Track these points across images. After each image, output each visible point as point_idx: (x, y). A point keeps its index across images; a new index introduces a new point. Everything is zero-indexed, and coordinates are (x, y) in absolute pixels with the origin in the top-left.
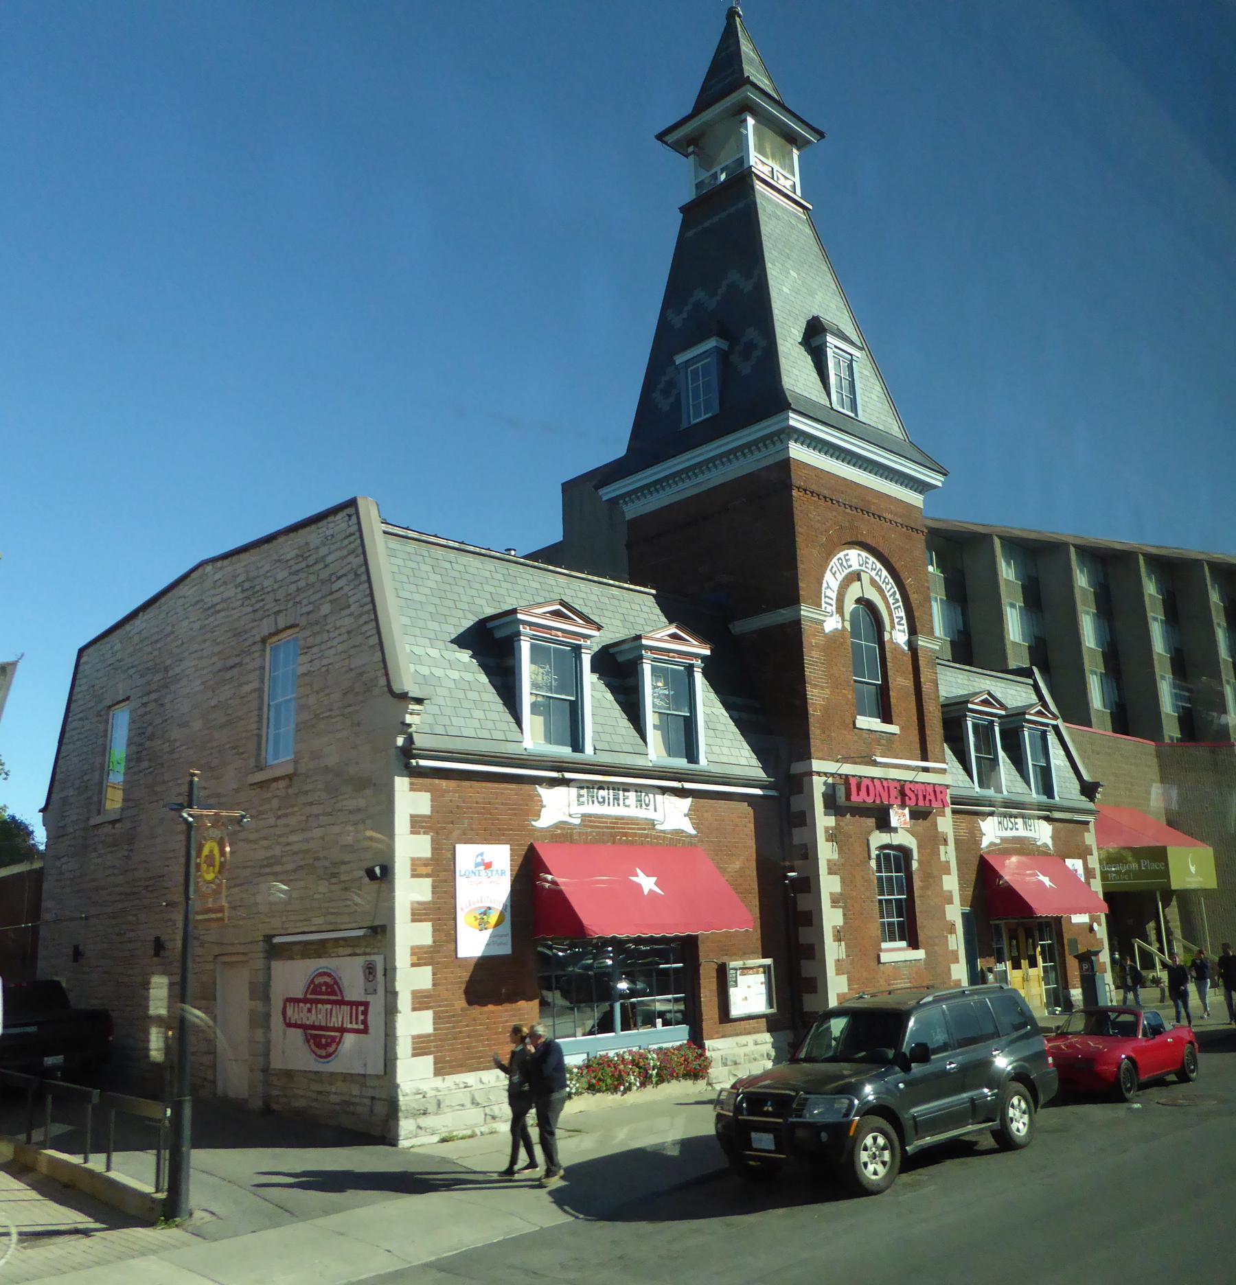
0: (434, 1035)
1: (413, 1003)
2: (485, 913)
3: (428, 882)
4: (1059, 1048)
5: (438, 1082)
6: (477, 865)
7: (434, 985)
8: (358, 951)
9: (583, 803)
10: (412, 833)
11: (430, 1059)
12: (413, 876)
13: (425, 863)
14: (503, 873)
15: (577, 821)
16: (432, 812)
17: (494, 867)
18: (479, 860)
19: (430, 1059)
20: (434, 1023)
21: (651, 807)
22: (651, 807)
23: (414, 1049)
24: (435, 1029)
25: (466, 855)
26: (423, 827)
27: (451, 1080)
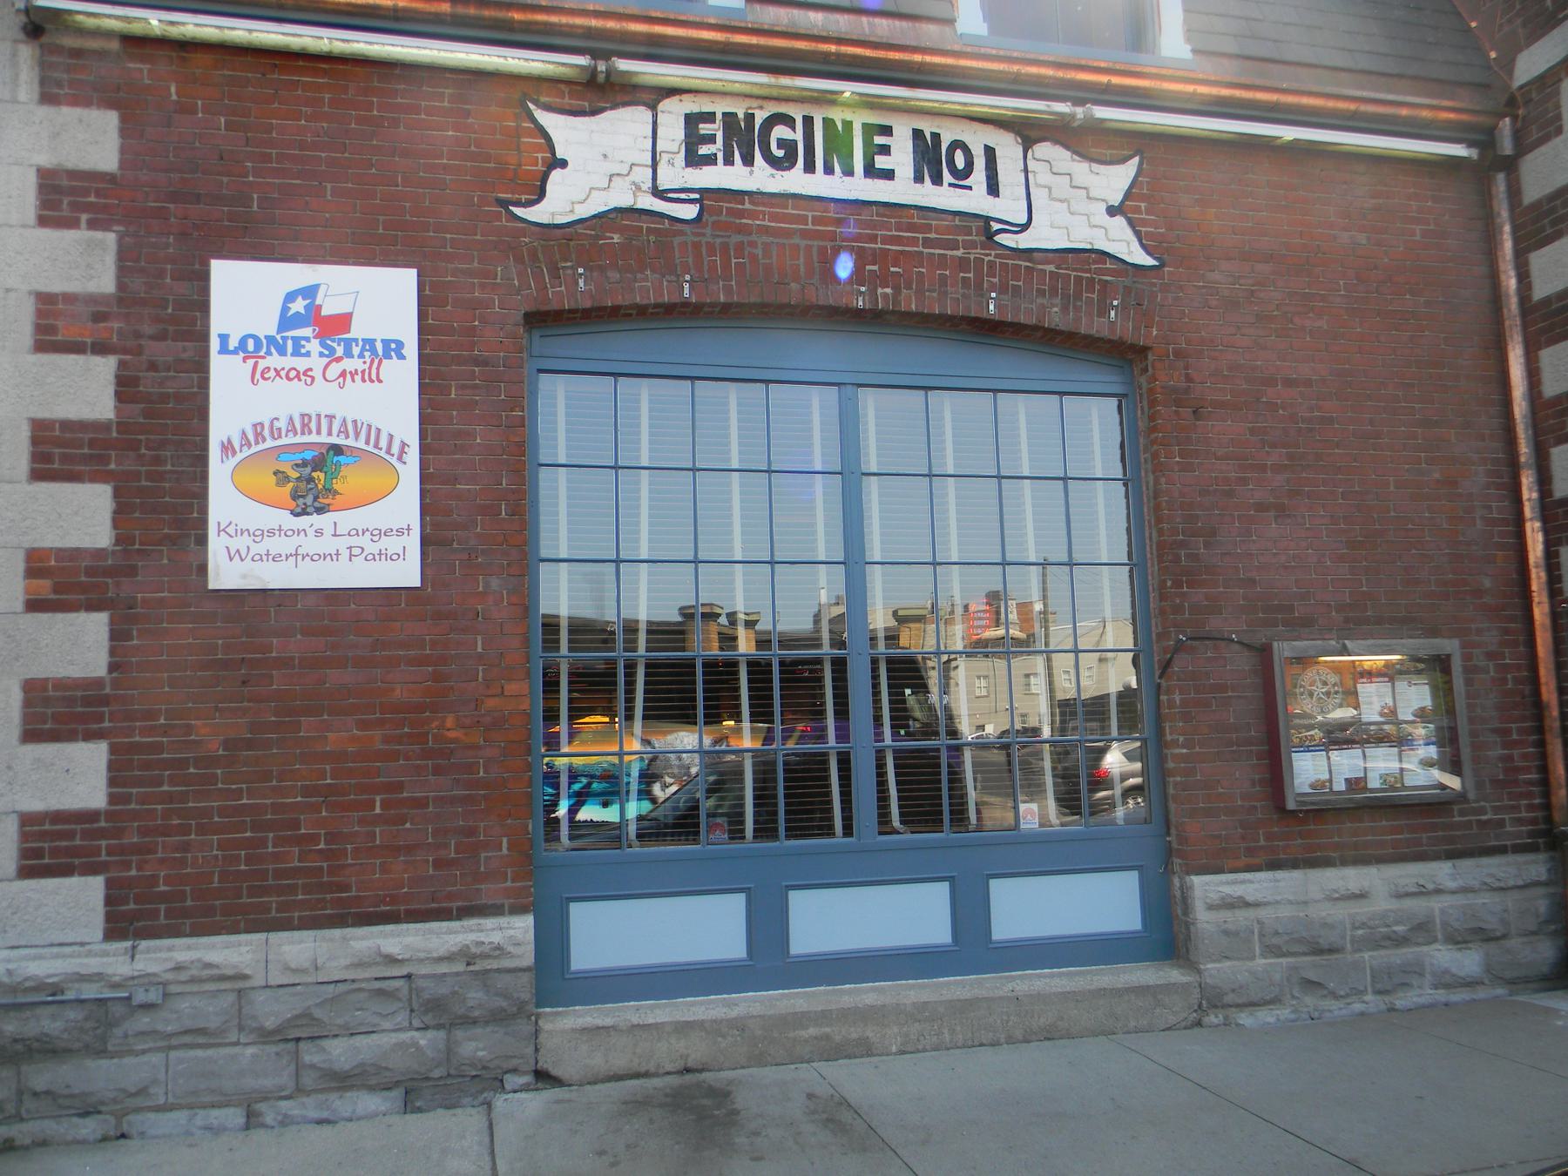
0: (109, 815)
1: (27, 718)
2: (318, 464)
3: (104, 368)
4: (415, 1044)
5: (117, 962)
6: (287, 322)
7: (112, 667)
8: (674, 1081)
9: (710, 160)
10: (43, 221)
11: (89, 891)
12: (41, 347)
13: (98, 309)
14: (393, 348)
15: (689, 212)
16: (123, 164)
17: (357, 331)
18: (299, 306)
19: (89, 891)
20: (112, 782)
21: (979, 177)
22: (979, 177)
23: (25, 854)
24: (113, 799)
25: (374, 544)
26: (88, 208)
27: (161, 956)
